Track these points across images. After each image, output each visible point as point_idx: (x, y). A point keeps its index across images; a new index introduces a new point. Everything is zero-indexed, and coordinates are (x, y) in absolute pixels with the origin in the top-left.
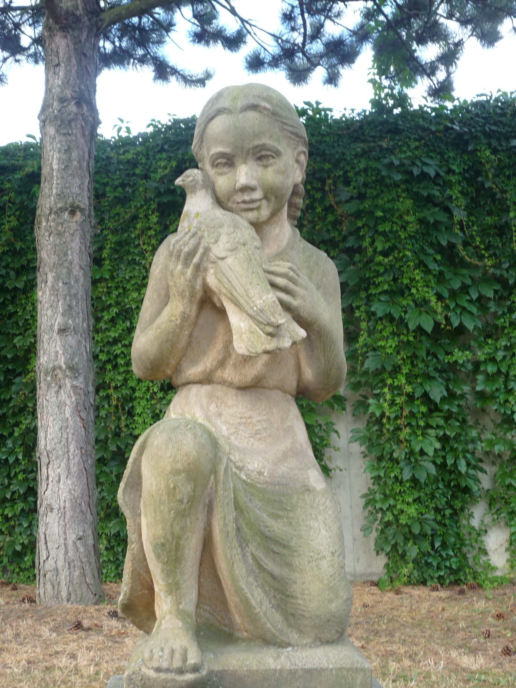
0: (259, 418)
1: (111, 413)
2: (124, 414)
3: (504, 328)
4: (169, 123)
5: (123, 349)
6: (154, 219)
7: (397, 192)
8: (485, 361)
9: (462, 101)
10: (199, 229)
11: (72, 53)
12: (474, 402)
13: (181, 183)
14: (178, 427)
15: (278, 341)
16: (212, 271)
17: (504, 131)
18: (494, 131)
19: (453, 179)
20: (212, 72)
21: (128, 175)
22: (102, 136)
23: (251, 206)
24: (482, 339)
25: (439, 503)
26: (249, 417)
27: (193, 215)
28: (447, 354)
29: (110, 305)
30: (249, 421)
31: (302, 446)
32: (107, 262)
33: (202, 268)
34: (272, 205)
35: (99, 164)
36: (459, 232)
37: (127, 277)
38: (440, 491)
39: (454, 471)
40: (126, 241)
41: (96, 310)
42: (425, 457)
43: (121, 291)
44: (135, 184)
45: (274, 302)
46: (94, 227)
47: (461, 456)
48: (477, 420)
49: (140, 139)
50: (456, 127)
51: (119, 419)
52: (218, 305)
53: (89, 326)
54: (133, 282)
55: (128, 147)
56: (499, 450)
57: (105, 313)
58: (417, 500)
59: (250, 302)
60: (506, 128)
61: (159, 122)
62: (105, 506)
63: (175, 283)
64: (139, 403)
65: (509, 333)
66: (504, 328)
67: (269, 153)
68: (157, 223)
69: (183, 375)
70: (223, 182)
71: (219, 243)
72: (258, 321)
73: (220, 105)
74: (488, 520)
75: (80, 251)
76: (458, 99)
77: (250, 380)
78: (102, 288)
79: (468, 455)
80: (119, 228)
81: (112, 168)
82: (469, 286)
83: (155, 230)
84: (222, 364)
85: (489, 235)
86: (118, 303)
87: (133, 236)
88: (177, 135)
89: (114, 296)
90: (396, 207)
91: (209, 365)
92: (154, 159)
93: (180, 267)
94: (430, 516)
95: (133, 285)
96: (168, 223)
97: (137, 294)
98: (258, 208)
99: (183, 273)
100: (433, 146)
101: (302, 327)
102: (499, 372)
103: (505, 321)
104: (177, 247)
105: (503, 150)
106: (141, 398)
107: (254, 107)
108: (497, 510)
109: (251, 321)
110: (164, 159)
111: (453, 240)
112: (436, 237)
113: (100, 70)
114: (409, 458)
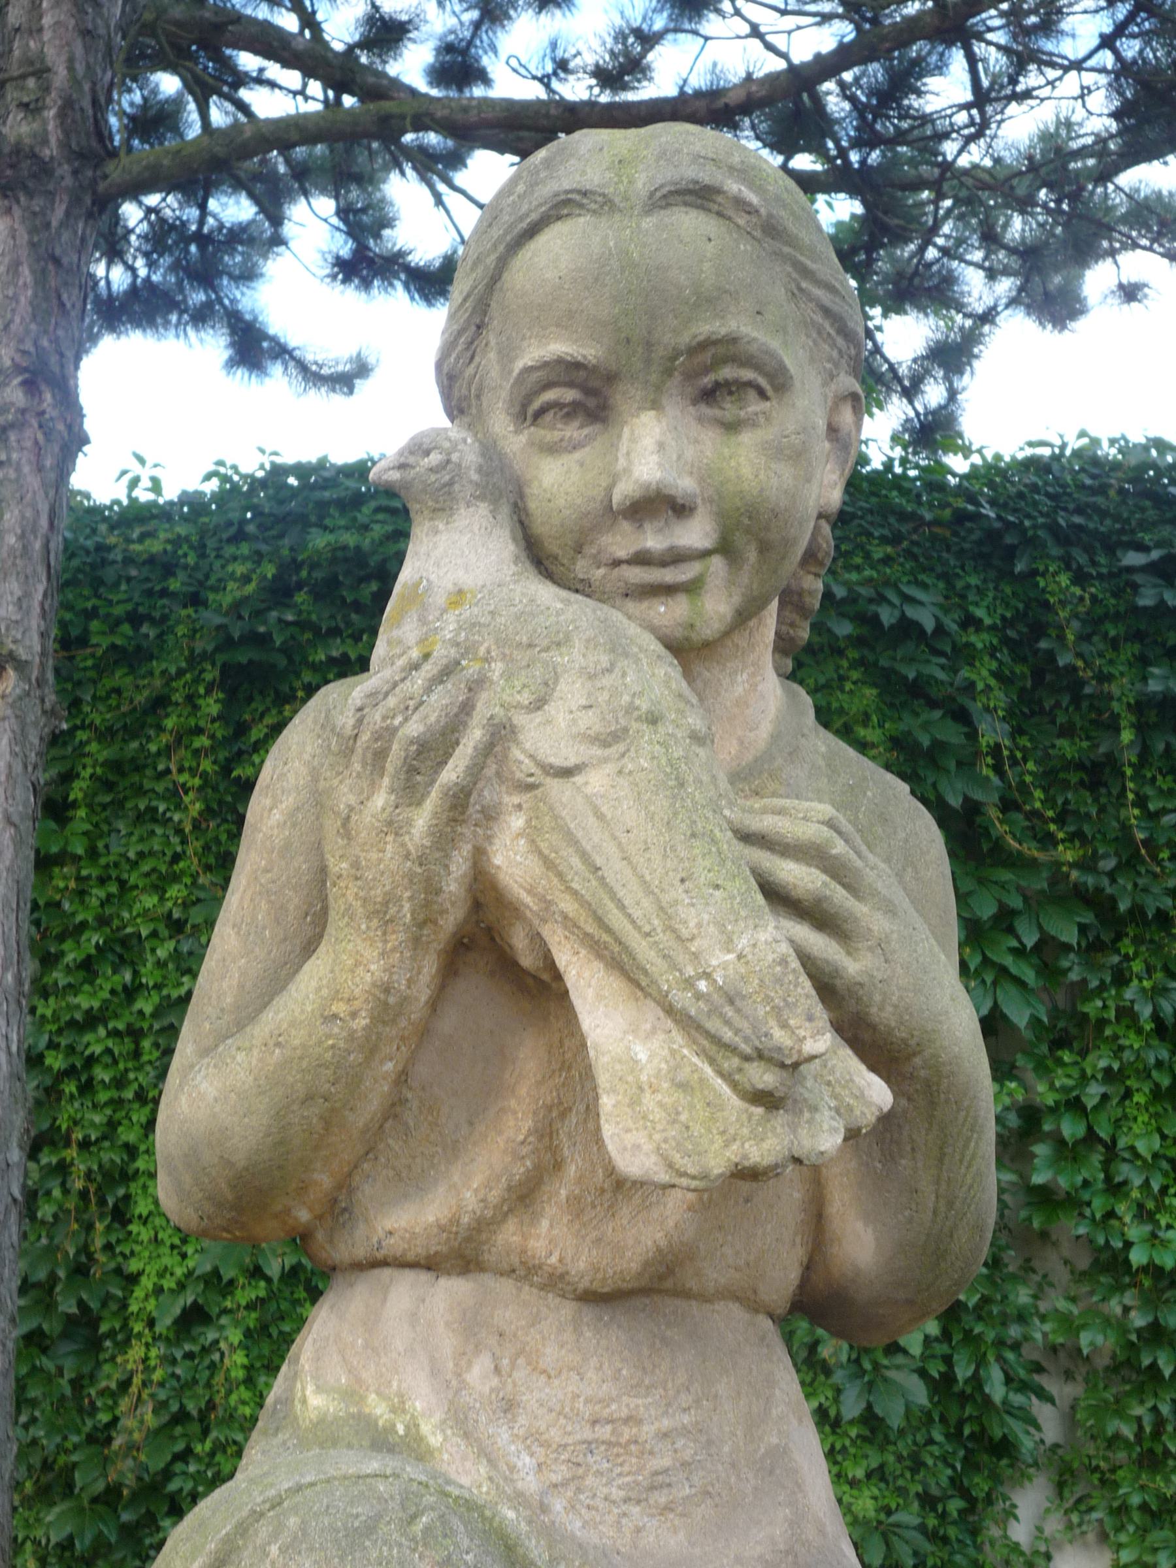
0: (666, 1423)
1: (68, 1211)
2: (102, 1216)
3: (1102, 1023)
4: (260, 474)
5: (110, 1043)
6: (211, 706)
7: (838, 667)
8: (1054, 1110)
10: (468, 650)
11: (24, 253)
12: (1023, 1214)
14: (370, 1529)
15: (793, 1128)
16: (517, 822)
18: (1080, 527)
19: (979, 640)
20: (371, 360)
21: (149, 593)
22: (88, 496)
23: (669, 576)
24: (1044, 1049)
25: (932, 1482)
26: (627, 1421)
29: (83, 925)
30: (627, 1433)
31: (822, 1532)
32: (82, 813)
33: (473, 810)
34: (745, 578)
35: (75, 562)
36: (991, 774)
37: (132, 855)
38: (936, 1450)
39: (972, 1396)
40: (133, 760)
41: (44, 936)
42: (900, 1359)
43: (113, 889)
44: (164, 618)
45: (783, 962)
46: (50, 714)
47: (991, 1358)
48: (1028, 1260)
50: (988, 511)
51: (89, 1227)
52: (527, 961)
53: (19, 981)
54: (146, 867)
56: (1092, 1344)
57: (68, 945)
58: (878, 1474)
59: (681, 958)
61: (235, 468)
62: (38, 1466)
63: (356, 865)
65: (1116, 1037)
66: (1102, 1023)
67: (747, 374)
68: (219, 717)
69: (361, 1231)
74: (1054, 1525)
75: (9, 775)
76: (979, 451)
77: (635, 1266)
78: (63, 878)
79: (1010, 1356)
80: (118, 726)
81: (110, 574)
82: (1013, 913)
83: (212, 737)
84: (524, 1196)
85: (1066, 785)
86: (103, 922)
87: (153, 748)
88: (281, 502)
89: (94, 902)
90: (835, 705)
91: (470, 1199)
92: (218, 557)
93: (381, 800)
94: (909, 1516)
95: (147, 875)
97: (155, 899)
98: (692, 588)
99: (393, 826)
100: (929, 558)
101: (873, 1068)
102: (1091, 1136)
103: (1105, 1007)
105: (1100, 576)
108: (1079, 1501)
109: (678, 1038)
110: (245, 559)
111: (978, 795)
112: (934, 785)
113: (94, 339)
114: (857, 1361)
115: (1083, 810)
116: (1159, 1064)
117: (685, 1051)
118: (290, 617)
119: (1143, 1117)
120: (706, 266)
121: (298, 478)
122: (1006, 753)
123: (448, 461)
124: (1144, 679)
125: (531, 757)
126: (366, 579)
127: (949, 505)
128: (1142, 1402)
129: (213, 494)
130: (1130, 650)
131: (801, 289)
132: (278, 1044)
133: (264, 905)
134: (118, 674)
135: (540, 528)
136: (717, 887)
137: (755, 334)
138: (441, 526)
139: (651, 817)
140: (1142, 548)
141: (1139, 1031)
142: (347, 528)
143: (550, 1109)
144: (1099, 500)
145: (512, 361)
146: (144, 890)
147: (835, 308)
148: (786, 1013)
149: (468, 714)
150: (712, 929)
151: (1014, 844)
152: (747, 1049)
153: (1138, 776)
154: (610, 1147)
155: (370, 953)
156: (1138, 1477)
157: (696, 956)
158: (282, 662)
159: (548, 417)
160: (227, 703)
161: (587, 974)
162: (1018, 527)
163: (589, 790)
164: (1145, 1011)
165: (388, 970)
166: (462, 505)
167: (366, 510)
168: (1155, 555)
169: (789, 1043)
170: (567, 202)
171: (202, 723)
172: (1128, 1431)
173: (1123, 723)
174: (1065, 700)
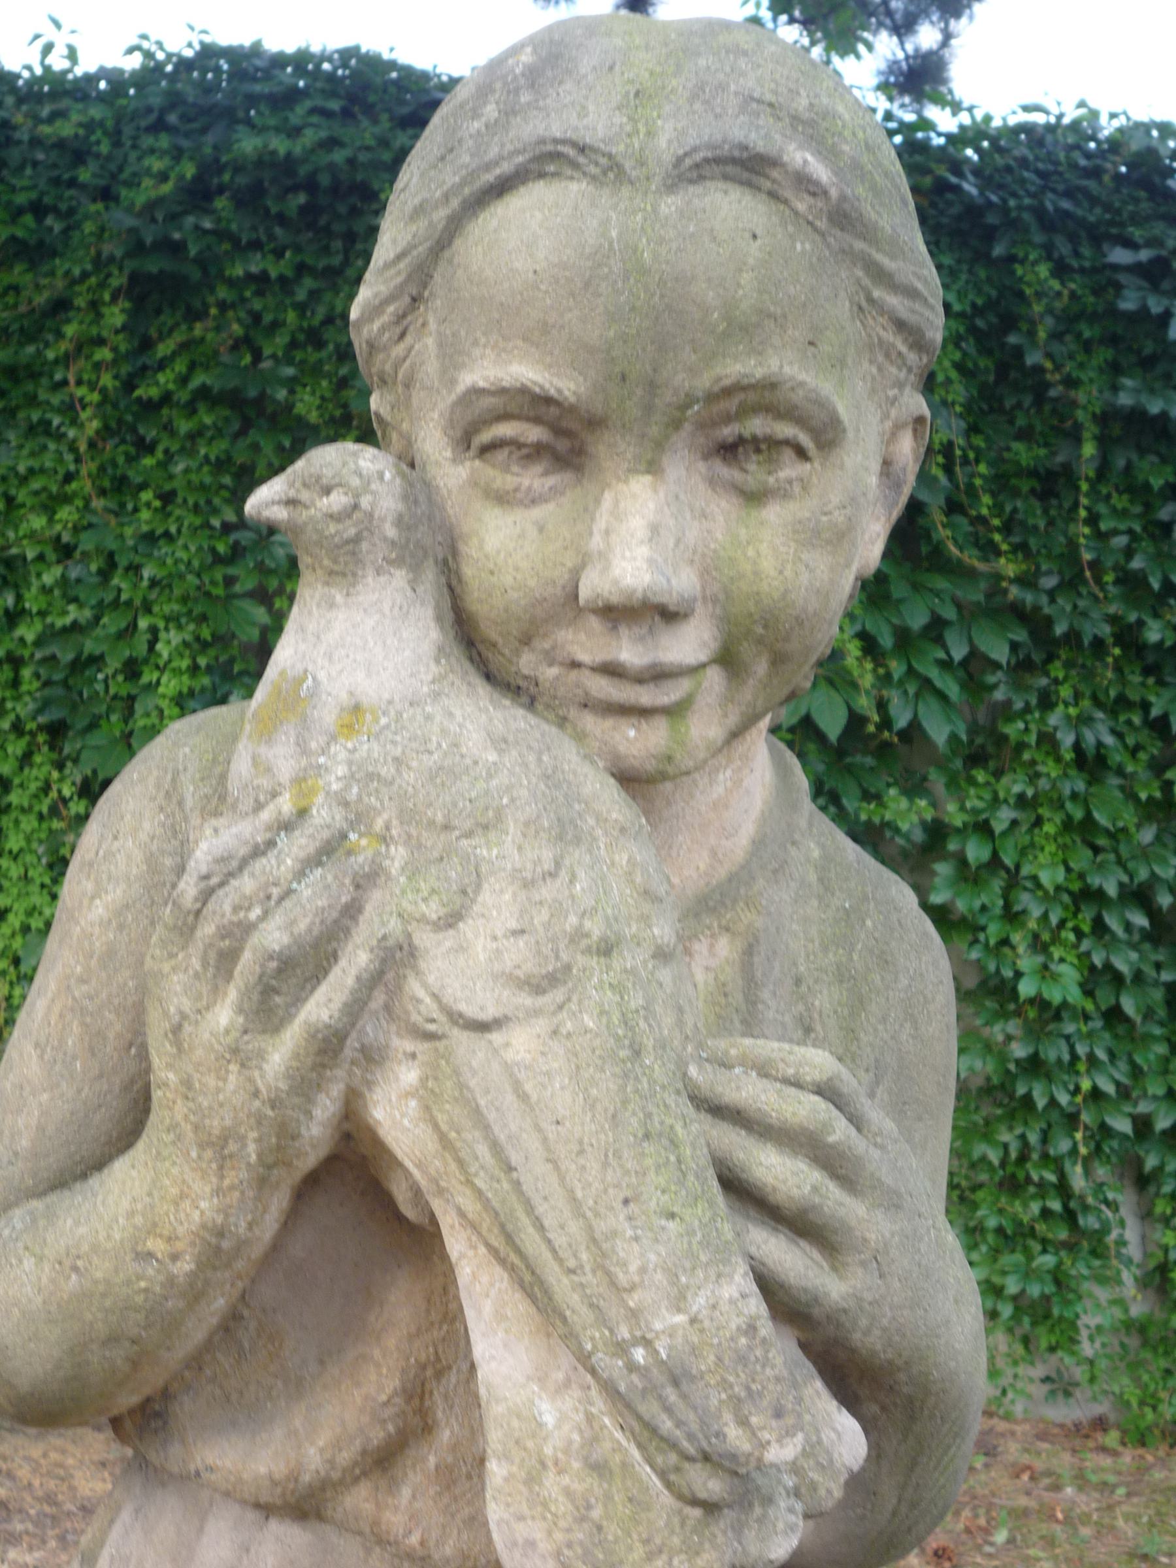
3: (1021, 746)
4: (189, 53)
6: (115, 316)
8: (961, 832)
9: (979, 115)
10: (359, 818)
13: (279, 514)
15: (738, 1529)
16: (409, 1075)
17: (1092, 219)
18: (1067, 214)
21: (56, 182)
23: (645, 696)
24: (958, 764)
27: (327, 715)
28: (868, 796)
40: (28, 366)
44: (71, 211)
45: (751, 1329)
49: (103, 85)
50: (970, 187)
52: (408, 1211)
54: (36, 485)
55: (65, 103)
59: (614, 1312)
60: (1098, 210)
61: (160, 45)
63: (187, 1083)
64: (17, 822)
66: (1021, 746)
67: (785, 430)
68: (124, 328)
69: (175, 1450)
70: (509, 542)
71: (466, 927)
72: (654, 1431)
73: (553, 121)
76: (970, 109)
80: (15, 327)
83: (114, 349)
84: (383, 1461)
85: (1015, 493)
87: (50, 355)
93: (224, 1016)
95: (36, 493)
96: (153, 332)
99: (240, 1056)
102: (995, 861)
103: (1027, 729)
104: (224, 904)
105: (1082, 271)
106: (23, 810)
107: (748, 167)
109: (599, 1404)
110: (163, 153)
115: (1031, 521)
116: (1074, 796)
117: (607, 1421)
118: (207, 224)
119: (1051, 848)
120: (746, 278)
121: (230, 62)
122: (958, 452)
123: (356, 507)
124: (1115, 388)
125: (435, 996)
126: (295, 189)
127: (929, 171)
128: (1011, 1129)
129: (134, 73)
130: (1104, 354)
131: (871, 300)
132: (75, 1269)
133: (76, 1027)
134: (18, 269)
135: (476, 602)
136: (672, 1216)
137: (803, 376)
138: (339, 598)
139: (591, 1104)
140: (1129, 244)
141: (1058, 759)
142: (277, 130)
143: (423, 1367)
144: (1091, 184)
145: (458, 367)
146: (32, 509)
147: (912, 319)
148: (747, 1408)
149: (354, 918)
150: (659, 1276)
151: (954, 550)
152: (692, 1451)
153: (1094, 491)
154: (495, 1536)
155: (201, 1187)
156: (998, 1200)
157: (634, 1315)
158: (196, 274)
159: (502, 455)
160: (134, 314)
161: (485, 1279)
162: (1005, 210)
163: (509, 1056)
164: (1067, 739)
165: (225, 1211)
166: (370, 572)
167: (300, 110)
168: (1144, 255)
169: (746, 1447)
170: (555, 156)
171: (105, 334)
172: (994, 1157)
173: (1086, 435)
174: (1027, 400)
